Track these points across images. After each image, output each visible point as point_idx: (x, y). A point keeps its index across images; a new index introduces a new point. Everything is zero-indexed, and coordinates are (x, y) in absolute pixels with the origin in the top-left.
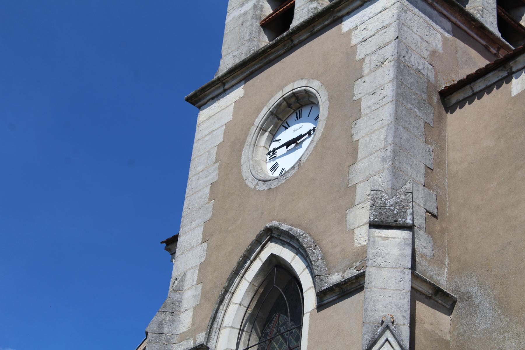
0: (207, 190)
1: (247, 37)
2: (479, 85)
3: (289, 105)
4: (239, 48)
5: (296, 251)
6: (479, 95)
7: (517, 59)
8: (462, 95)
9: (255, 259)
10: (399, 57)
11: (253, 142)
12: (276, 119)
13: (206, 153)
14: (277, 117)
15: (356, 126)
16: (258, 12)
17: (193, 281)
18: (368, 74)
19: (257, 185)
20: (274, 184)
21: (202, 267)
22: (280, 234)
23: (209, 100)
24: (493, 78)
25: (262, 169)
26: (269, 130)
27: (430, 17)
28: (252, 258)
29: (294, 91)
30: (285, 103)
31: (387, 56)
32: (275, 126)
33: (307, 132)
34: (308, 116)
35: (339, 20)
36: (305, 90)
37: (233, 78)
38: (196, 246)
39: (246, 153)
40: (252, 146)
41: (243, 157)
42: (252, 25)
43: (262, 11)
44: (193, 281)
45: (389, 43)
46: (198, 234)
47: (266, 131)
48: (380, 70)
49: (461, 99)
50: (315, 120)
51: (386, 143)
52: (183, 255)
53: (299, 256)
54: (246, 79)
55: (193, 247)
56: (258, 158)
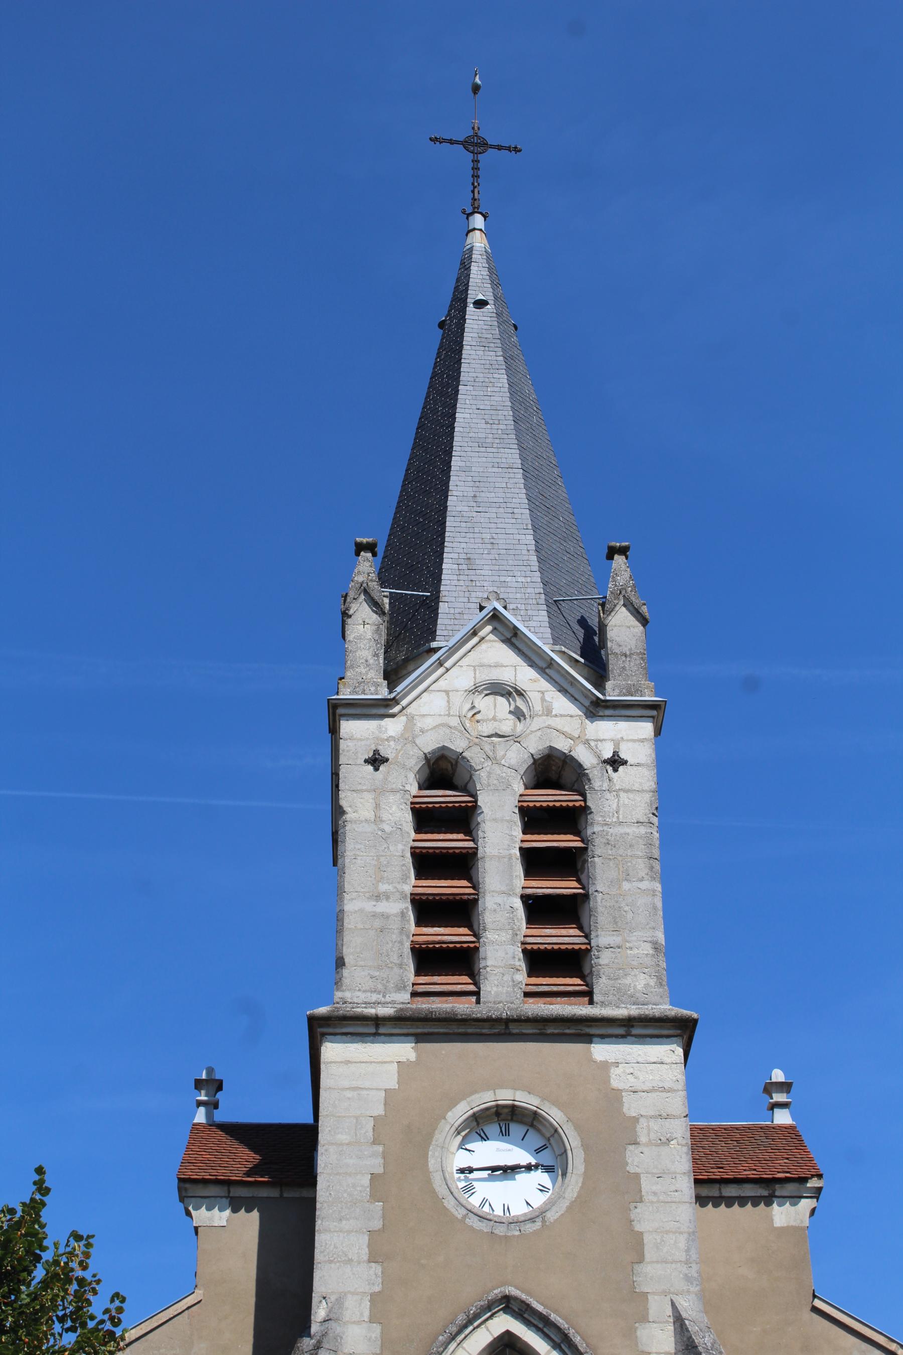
0: (366, 1180)
2: (731, 1191)
5: (552, 1344)
6: (730, 1202)
7: (785, 1185)
8: (706, 1191)
9: (478, 1326)
13: (352, 1119)
15: (636, 1210)
19: (465, 1216)
22: (524, 1310)
23: (346, 1034)
24: (749, 1190)
28: (476, 1324)
29: (516, 1103)
33: (525, 1164)
34: (523, 1140)
35: (588, 1039)
36: (536, 1111)
37: (395, 1027)
38: (359, 1263)
44: (362, 1314)
46: (359, 1246)
47: (459, 1133)
49: (703, 1195)
50: (535, 1151)
51: (688, 1257)
53: (557, 1352)
54: (420, 1038)
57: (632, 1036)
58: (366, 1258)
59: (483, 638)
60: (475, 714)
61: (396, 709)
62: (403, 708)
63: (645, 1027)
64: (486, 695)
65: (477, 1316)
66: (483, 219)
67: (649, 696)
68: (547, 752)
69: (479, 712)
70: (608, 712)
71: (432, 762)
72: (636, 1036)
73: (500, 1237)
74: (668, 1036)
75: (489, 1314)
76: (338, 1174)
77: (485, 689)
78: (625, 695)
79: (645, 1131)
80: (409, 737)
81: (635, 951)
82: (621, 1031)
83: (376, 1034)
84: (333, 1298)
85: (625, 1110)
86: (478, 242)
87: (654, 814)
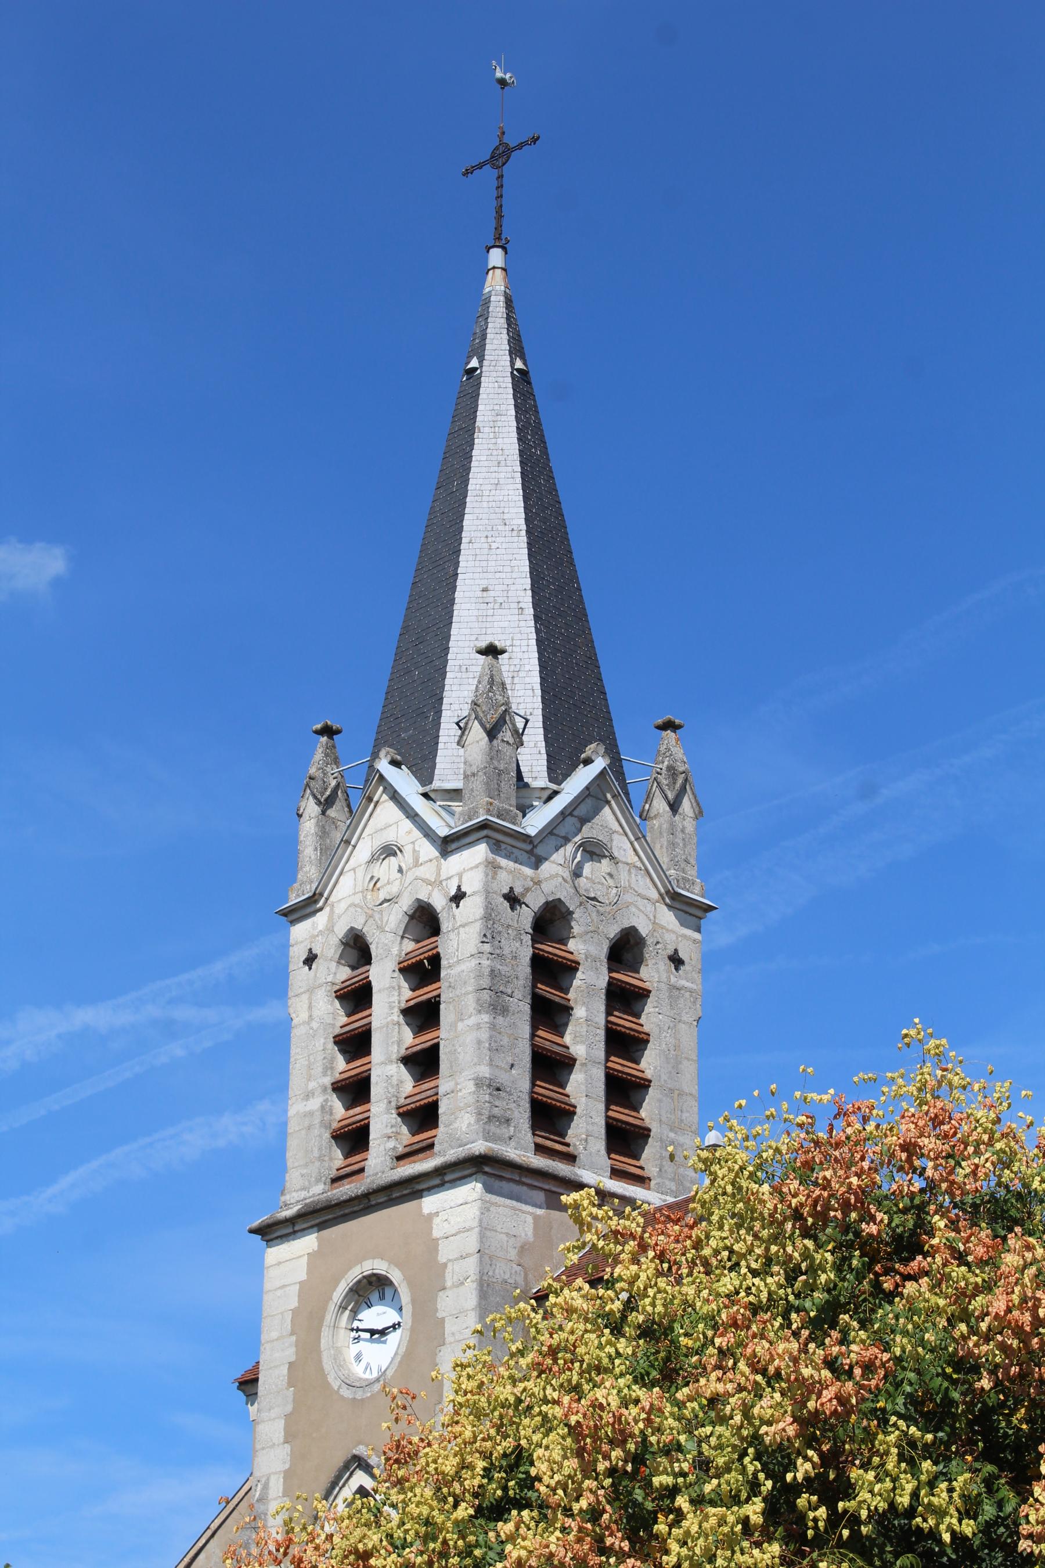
0: (285, 1370)
1: (316, 1154)
3: (370, 1283)
4: (306, 1165)
9: (344, 1486)
10: (481, 1278)
11: (332, 1324)
12: (357, 1296)
14: (358, 1293)
16: (327, 1117)
17: (278, 1492)
18: (451, 1288)
20: (360, 1394)
21: (288, 1475)
23: (277, 1238)
25: (344, 1360)
26: (350, 1308)
27: (518, 1199)
28: (340, 1484)
30: (365, 1280)
31: (469, 1274)
32: (356, 1303)
34: (466, 173)
35: (418, 1195)
38: (278, 1445)
39: (325, 1333)
40: (331, 1328)
41: (323, 1341)
42: (320, 1136)
43: (331, 1114)
44: (278, 1492)
45: (468, 1255)
47: (346, 1309)
48: (462, 1288)
52: (264, 1452)
54: (321, 1226)
55: (274, 1444)
56: (339, 1344)
57: (447, 1182)
58: (282, 1440)
59: (377, 802)
60: (376, 883)
61: (321, 904)
62: (327, 899)
63: (453, 1171)
64: (384, 859)
65: (338, 1478)
66: (503, 253)
67: (483, 815)
68: (417, 905)
69: (379, 879)
70: (454, 846)
71: (352, 943)
72: (450, 1182)
73: (359, 1400)
74: (470, 1175)
75: (348, 1474)
76: (271, 1368)
77: (381, 854)
78: (467, 822)
79: (451, 1274)
80: (330, 929)
81: (464, 1091)
82: (437, 1181)
83: (295, 1232)
84: (263, 1480)
85: (439, 1258)
86: (495, 284)
87: (483, 942)
